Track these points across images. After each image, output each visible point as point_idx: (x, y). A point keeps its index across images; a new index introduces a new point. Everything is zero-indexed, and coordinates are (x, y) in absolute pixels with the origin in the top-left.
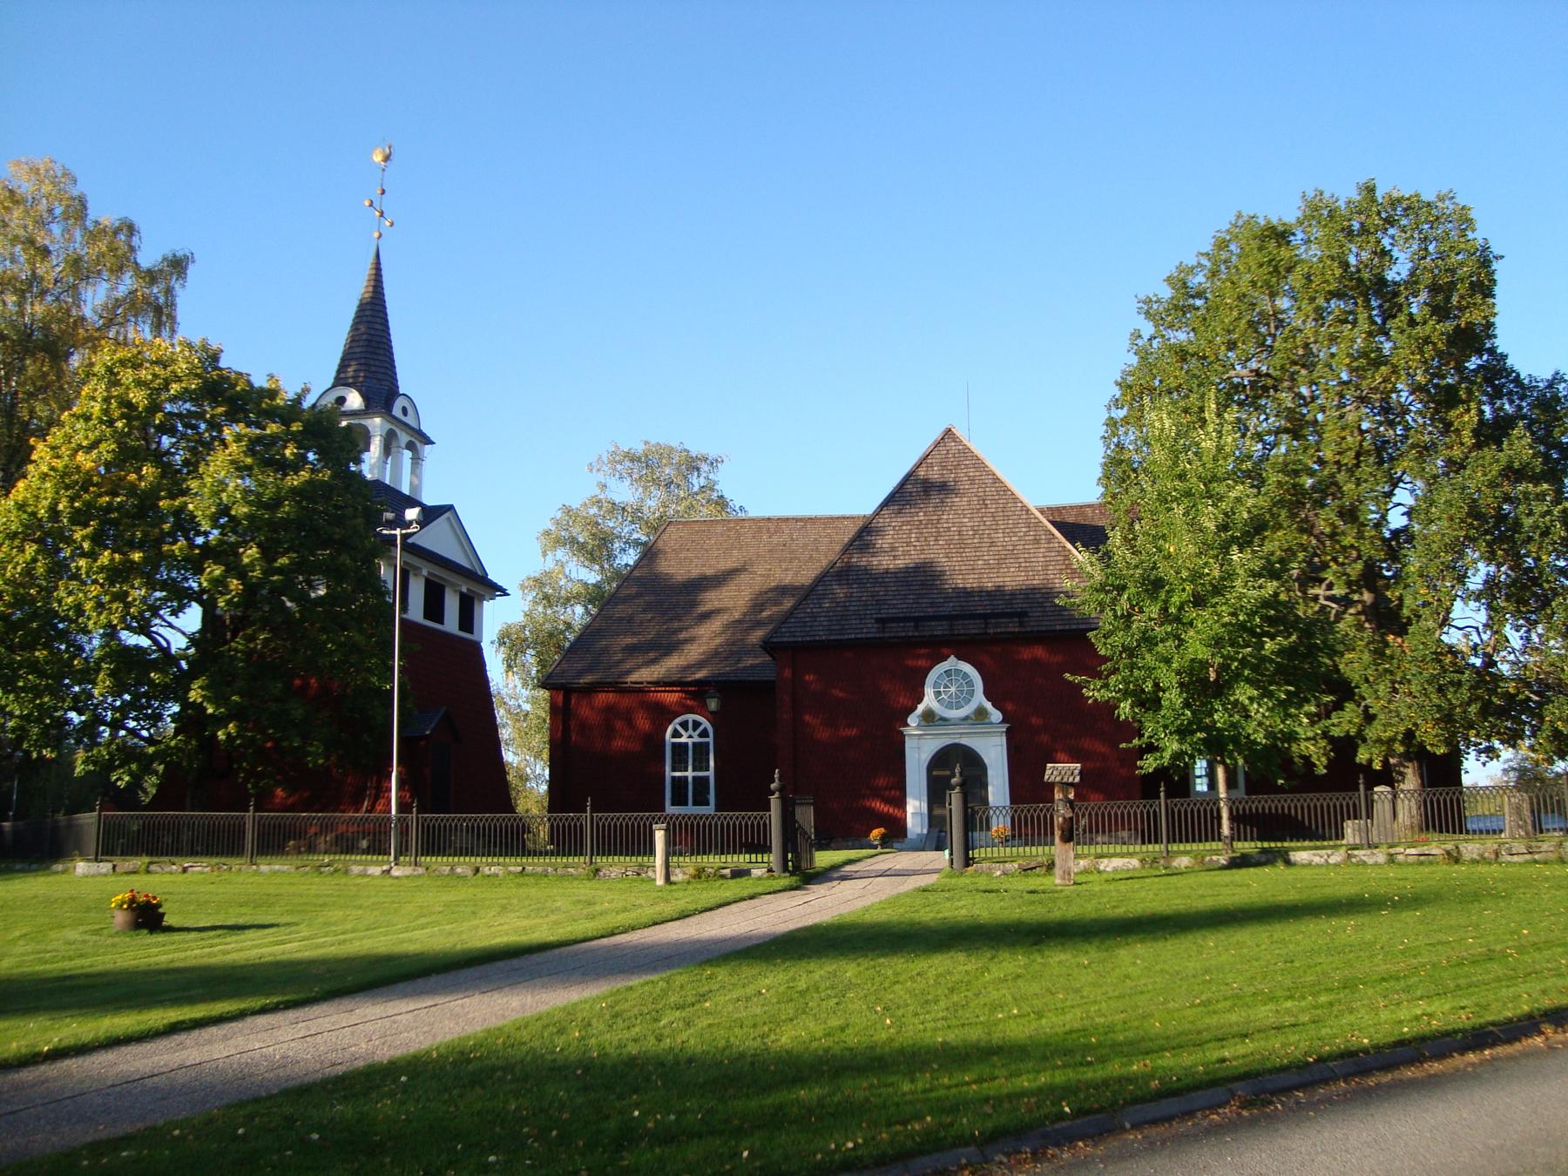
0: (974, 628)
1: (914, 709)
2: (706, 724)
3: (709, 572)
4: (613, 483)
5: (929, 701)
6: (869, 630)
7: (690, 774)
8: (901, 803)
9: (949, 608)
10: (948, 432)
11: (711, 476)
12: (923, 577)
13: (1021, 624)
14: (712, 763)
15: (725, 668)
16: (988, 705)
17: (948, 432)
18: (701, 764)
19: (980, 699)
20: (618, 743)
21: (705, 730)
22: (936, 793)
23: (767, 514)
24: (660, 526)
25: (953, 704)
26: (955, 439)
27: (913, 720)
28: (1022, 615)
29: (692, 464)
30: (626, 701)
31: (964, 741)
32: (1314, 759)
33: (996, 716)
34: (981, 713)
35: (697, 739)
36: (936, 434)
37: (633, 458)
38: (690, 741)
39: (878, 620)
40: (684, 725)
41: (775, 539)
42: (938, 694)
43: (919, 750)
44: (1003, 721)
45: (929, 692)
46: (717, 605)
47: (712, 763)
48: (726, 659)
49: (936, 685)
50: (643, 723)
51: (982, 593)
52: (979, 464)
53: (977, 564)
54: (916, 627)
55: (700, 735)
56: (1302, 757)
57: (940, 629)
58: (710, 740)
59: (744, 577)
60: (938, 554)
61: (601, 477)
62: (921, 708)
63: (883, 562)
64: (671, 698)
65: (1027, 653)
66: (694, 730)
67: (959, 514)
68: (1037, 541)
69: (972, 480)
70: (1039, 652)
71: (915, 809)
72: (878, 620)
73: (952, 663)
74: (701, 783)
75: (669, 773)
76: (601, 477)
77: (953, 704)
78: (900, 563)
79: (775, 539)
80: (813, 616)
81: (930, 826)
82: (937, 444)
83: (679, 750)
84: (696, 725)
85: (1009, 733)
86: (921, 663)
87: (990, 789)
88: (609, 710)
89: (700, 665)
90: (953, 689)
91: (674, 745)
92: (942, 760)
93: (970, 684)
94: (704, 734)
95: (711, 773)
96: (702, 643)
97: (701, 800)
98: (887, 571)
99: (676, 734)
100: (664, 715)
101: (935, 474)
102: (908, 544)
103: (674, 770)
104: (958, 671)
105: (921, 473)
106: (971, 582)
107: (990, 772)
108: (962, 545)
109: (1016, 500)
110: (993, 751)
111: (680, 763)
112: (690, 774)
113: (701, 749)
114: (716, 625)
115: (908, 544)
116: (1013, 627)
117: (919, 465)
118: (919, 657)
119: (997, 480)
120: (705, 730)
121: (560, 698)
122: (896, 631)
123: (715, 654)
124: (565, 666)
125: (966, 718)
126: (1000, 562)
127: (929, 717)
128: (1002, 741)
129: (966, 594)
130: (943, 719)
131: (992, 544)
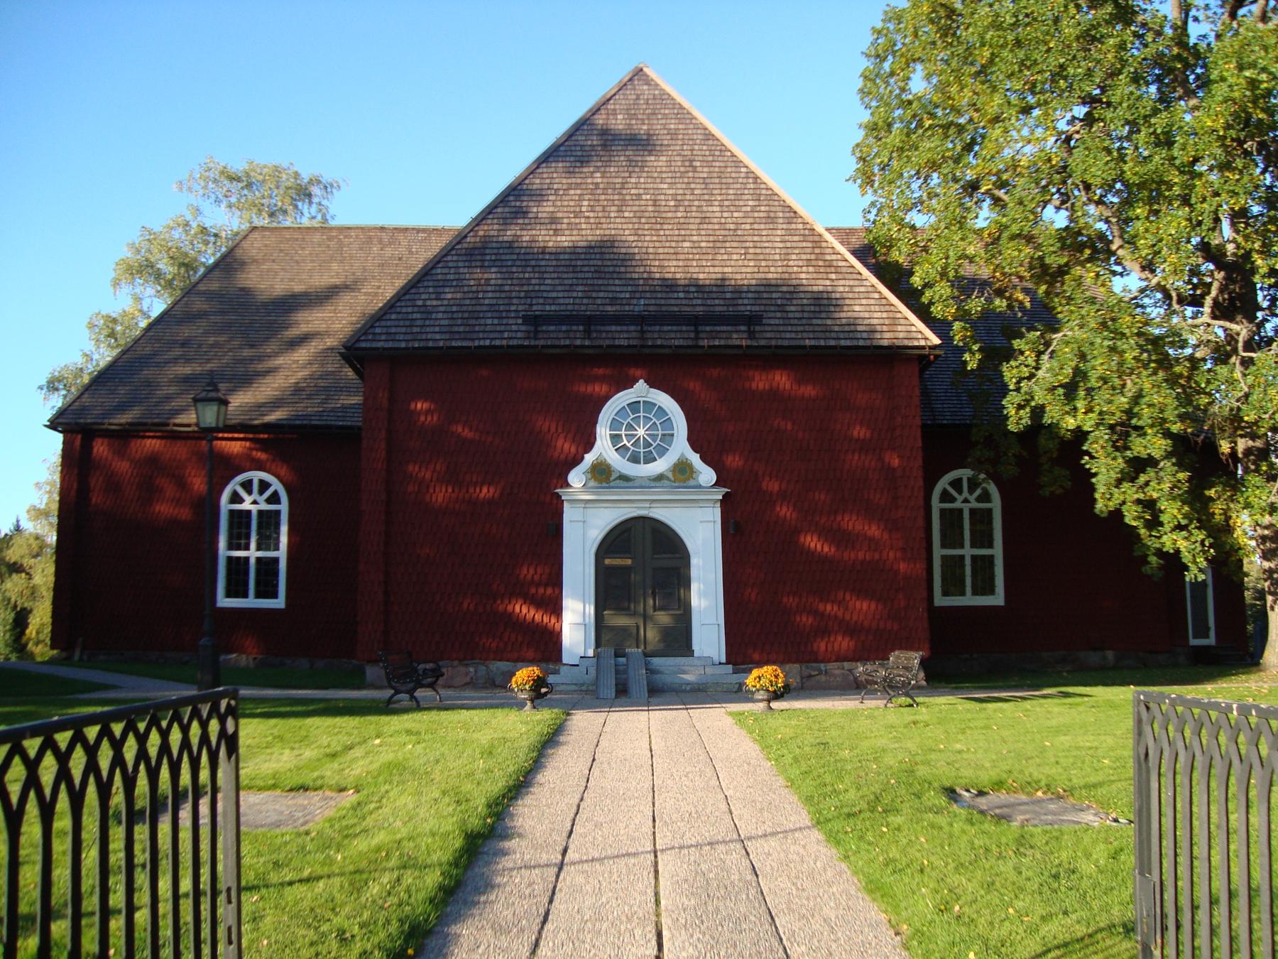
0: (676, 337)
1: (577, 460)
2: (276, 485)
3: (298, 288)
4: (207, 206)
5: (603, 449)
6: (514, 334)
7: (253, 553)
8: (557, 610)
9: (639, 306)
10: (639, 72)
11: (325, 202)
12: (602, 260)
13: (751, 334)
14: (284, 539)
15: (310, 408)
16: (695, 459)
17: (639, 72)
18: (268, 540)
19: (681, 447)
20: (163, 509)
21: (275, 494)
22: (611, 590)
23: (380, 223)
24: (239, 240)
25: (639, 463)
26: (648, 81)
27: (576, 478)
28: (752, 320)
29: (303, 193)
30: (180, 450)
31: (660, 513)
32: (1186, 557)
33: (707, 475)
34: (683, 469)
35: (264, 506)
36: (623, 73)
37: (233, 178)
38: (254, 508)
39: (528, 320)
40: (247, 485)
41: (388, 252)
42: (615, 438)
43: (585, 524)
44: (717, 484)
45: (603, 432)
46: (304, 328)
47: (284, 539)
48: (309, 397)
49: (615, 424)
50: (198, 483)
51: (697, 288)
52: (682, 114)
53: (687, 249)
54: (588, 333)
55: (269, 501)
56: (1160, 553)
57: (624, 337)
58: (284, 507)
59: (347, 298)
60: (621, 228)
61: (192, 199)
62: (589, 458)
63: (544, 237)
64: (235, 447)
65: (760, 382)
66: (261, 493)
67: (657, 179)
68: (770, 219)
69: (673, 135)
70: (782, 380)
71: (576, 621)
72: (528, 320)
73: (640, 390)
74: (268, 567)
75: (997, 551)
76: (192, 199)
77: (639, 463)
78: (565, 240)
79: (388, 252)
80: (427, 312)
81: (598, 644)
82: (622, 87)
83: (240, 520)
84: (264, 486)
85: (726, 502)
86: (599, 389)
87: (694, 587)
88: (153, 461)
89: (276, 404)
90: (641, 432)
91: (232, 512)
92: (619, 541)
93: (668, 423)
94: (274, 499)
95: (282, 553)
96: (283, 379)
97: (266, 590)
98: (543, 251)
99: (236, 498)
100: (225, 468)
101: (619, 123)
102: (577, 215)
103: (231, 547)
104: (649, 405)
105: (600, 120)
106: (674, 270)
107: (695, 561)
108: (659, 220)
109: (738, 163)
110: (701, 531)
111: (238, 538)
112: (253, 553)
113: (269, 521)
114: (302, 354)
115: (577, 215)
116: (739, 338)
117: (596, 111)
118: (597, 379)
119: (709, 136)
120: (275, 494)
121: (78, 442)
122: (556, 337)
123: (297, 390)
124: (86, 399)
125: (660, 478)
126: (717, 245)
127: (601, 472)
128: (716, 514)
129: (670, 286)
130: (624, 478)
131: (704, 220)
